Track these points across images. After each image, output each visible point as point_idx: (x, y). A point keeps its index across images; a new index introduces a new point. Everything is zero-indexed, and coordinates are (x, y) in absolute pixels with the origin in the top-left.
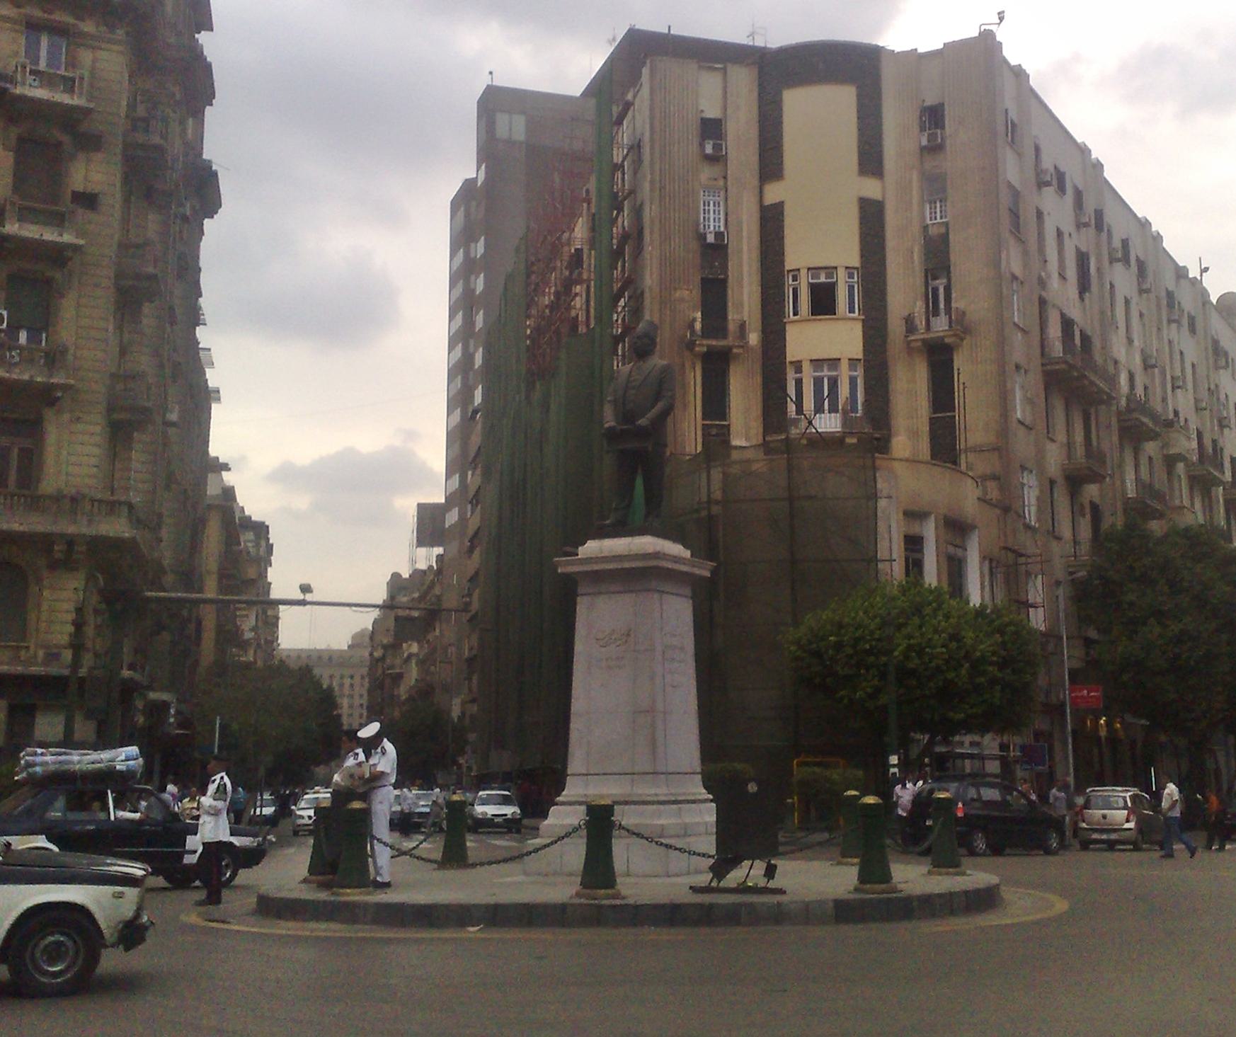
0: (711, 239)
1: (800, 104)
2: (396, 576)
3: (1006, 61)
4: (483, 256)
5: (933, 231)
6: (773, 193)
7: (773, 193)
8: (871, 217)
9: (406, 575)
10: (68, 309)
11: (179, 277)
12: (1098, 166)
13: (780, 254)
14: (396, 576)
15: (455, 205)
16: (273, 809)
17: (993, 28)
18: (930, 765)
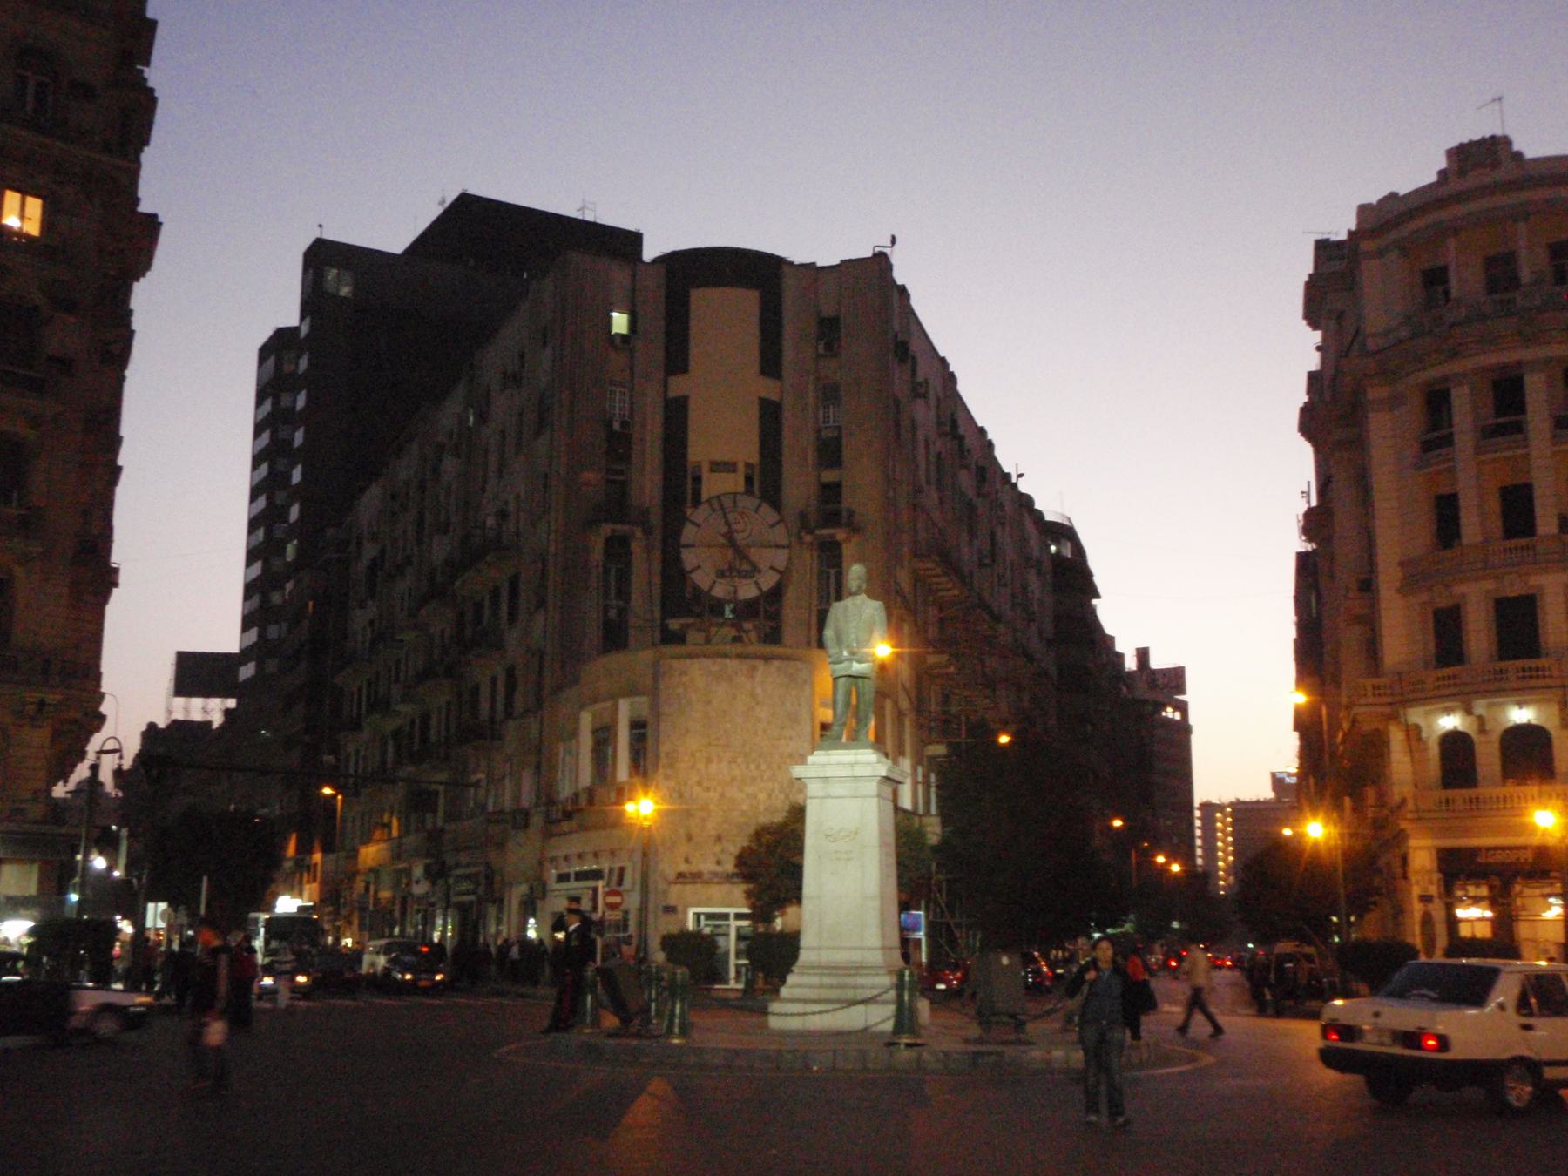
0: (616, 426)
1: (705, 302)
2: (152, 727)
3: (893, 281)
4: (303, 410)
5: (826, 434)
6: (678, 386)
7: (678, 386)
8: (770, 413)
9: (162, 724)
10: (1368, 916)
11: (541, 654)
12: (990, 445)
13: (683, 445)
14: (152, 727)
15: (265, 352)
16: (436, 940)
17: (887, 251)
18: (1220, 878)
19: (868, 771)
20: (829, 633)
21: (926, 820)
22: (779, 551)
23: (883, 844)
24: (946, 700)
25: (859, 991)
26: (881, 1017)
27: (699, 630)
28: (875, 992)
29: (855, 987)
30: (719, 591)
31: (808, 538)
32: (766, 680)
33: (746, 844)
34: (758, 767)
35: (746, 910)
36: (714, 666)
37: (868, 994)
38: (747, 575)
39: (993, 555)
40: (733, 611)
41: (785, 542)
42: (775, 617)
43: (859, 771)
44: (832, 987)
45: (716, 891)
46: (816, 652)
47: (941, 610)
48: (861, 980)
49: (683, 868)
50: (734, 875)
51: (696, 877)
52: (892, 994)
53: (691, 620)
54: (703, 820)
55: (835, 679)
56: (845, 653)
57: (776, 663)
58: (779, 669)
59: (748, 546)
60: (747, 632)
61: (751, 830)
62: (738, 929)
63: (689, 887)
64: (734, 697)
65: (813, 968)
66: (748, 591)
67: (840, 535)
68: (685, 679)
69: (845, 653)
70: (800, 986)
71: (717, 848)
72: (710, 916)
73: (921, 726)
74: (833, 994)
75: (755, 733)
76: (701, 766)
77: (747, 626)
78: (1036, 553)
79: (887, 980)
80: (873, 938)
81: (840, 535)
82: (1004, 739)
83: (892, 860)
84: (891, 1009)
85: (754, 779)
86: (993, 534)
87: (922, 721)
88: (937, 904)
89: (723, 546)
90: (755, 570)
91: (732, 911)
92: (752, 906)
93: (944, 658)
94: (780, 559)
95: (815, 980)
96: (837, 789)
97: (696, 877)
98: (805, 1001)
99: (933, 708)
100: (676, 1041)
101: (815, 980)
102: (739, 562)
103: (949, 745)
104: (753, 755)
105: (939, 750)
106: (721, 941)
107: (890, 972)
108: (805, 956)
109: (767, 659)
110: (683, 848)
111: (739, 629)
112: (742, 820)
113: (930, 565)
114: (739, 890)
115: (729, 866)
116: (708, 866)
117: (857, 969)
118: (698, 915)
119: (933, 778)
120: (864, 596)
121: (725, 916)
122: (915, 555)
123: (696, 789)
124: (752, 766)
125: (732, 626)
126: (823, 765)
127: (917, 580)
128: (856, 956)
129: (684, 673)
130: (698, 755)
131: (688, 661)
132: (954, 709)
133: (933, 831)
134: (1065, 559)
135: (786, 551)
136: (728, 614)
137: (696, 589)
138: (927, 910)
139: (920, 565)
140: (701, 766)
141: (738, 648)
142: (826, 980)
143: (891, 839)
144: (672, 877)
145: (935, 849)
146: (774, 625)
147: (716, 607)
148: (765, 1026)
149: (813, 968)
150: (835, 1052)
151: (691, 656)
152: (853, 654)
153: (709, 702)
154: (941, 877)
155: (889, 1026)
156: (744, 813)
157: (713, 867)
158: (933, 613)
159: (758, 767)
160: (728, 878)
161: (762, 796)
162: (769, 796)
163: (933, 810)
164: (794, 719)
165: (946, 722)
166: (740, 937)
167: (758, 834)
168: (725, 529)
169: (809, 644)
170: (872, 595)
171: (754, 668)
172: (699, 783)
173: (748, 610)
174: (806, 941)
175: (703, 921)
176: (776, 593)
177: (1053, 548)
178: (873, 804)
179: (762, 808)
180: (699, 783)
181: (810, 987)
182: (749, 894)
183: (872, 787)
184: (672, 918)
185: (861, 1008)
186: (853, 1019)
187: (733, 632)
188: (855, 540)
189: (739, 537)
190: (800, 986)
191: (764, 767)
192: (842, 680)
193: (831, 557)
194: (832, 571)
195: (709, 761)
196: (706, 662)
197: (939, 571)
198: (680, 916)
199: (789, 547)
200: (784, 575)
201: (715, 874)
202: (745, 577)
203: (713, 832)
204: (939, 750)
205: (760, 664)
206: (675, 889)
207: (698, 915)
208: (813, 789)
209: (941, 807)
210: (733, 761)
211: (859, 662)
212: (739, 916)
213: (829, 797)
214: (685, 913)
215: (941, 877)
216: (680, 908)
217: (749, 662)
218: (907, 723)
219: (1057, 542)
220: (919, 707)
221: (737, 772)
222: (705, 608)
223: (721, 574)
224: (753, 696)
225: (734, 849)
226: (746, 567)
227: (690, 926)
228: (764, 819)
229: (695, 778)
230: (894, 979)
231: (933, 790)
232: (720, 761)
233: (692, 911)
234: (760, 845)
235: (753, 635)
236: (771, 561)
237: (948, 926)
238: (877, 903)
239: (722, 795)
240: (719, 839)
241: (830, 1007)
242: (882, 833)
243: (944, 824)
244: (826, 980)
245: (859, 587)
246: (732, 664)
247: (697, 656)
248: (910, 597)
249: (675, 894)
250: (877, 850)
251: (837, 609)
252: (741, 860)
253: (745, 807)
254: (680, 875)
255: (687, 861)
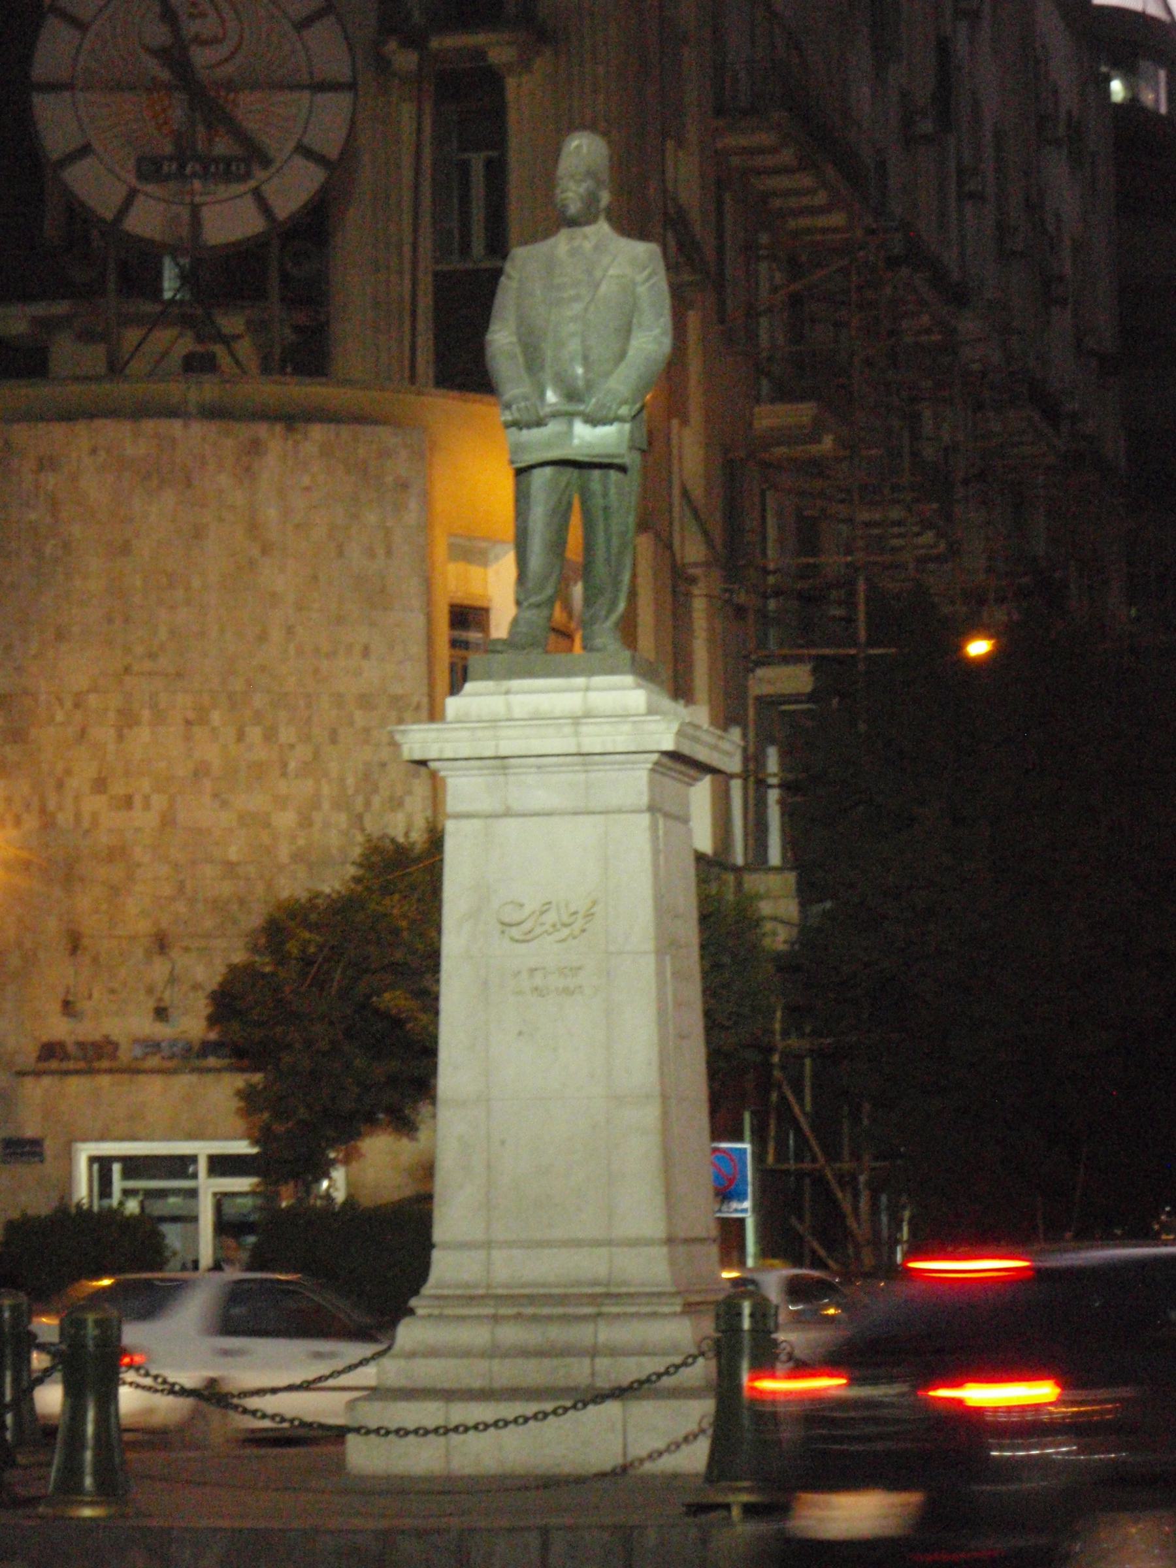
19: (620, 738)
20: (502, 338)
21: (755, 882)
22: (322, 98)
23: (666, 945)
24: (807, 536)
25: (602, 1363)
26: (669, 1436)
27: (87, 336)
28: (659, 1364)
29: (593, 1352)
30: (148, 219)
31: (405, 60)
32: (292, 481)
33: (239, 957)
34: (270, 735)
35: (242, 1147)
36: (132, 440)
37: (631, 1370)
38: (227, 171)
39: (946, 121)
40: (186, 278)
41: (340, 69)
42: (310, 297)
43: (594, 739)
44: (524, 1353)
45: (156, 1093)
46: (446, 409)
47: (795, 268)
48: (606, 1334)
49: (59, 1029)
50: (207, 1049)
51: (96, 1056)
52: (702, 1370)
53: (61, 308)
54: (115, 891)
55: (521, 472)
56: (551, 396)
57: (318, 432)
58: (326, 451)
59: (230, 85)
60: (227, 341)
61: (254, 920)
62: (220, 1199)
63: (75, 1085)
64: (198, 533)
65: (472, 1299)
66: (230, 219)
67: (499, 50)
68: (50, 480)
69: (551, 396)
70: (433, 1353)
71: (159, 970)
72: (134, 1166)
73: (740, 612)
74: (533, 1373)
75: (263, 637)
76: (104, 733)
77: (232, 323)
78: (1069, 101)
79: (681, 1332)
80: (641, 1211)
81: (499, 50)
82: (978, 648)
83: (693, 992)
84: (700, 1410)
85: (259, 771)
86: (943, 48)
87: (742, 598)
88: (786, 1117)
89: (154, 86)
90: (255, 155)
91: (203, 1149)
92: (262, 1137)
93: (803, 413)
94: (328, 121)
95: (476, 1335)
96: (537, 792)
97: (96, 1056)
98: (449, 1395)
99: (773, 556)
100: (87, 1512)
101: (476, 1335)
102: (205, 133)
103: (820, 665)
104: (259, 701)
105: (791, 679)
106: (172, 1235)
107: (690, 1309)
108: (446, 1268)
109: (292, 419)
110: (58, 973)
111: (206, 331)
112: (226, 889)
113: (766, 138)
114: (222, 1091)
115: (192, 1024)
116: (130, 1024)
117: (604, 1300)
118: (103, 1164)
119: (773, 763)
120: (603, 227)
121: (181, 1166)
122: (719, 112)
123: (94, 803)
124: (255, 734)
125: (186, 321)
126: (494, 722)
127: (723, 180)
128: (589, 1266)
129: (47, 464)
130: (93, 700)
131: (58, 430)
132: (833, 562)
133: (778, 904)
134: (1150, 115)
135: (343, 100)
136: (170, 286)
137: (77, 213)
138: (760, 1140)
139: (733, 141)
140: (104, 733)
141: (208, 390)
142: (511, 1334)
143: (689, 932)
144: (28, 1056)
145: (787, 965)
146: (338, 318)
147: (137, 268)
148: (340, 1464)
149: (472, 1299)
150: (545, 1531)
151: (68, 416)
152: (572, 395)
153: (125, 549)
154: (794, 1042)
155: (695, 1458)
156: (230, 868)
157: (143, 1024)
158: (769, 276)
159: (270, 735)
160: (191, 1057)
161: (286, 819)
162: (306, 822)
163: (775, 856)
164: (376, 596)
165: (808, 599)
166: (223, 1227)
167: (276, 931)
168: (159, 34)
169: (413, 379)
170: (631, 224)
171: (255, 447)
172: (100, 785)
173: (229, 277)
174: (451, 1221)
175: (118, 1184)
176: (313, 227)
177: (1117, 88)
178: (637, 833)
179: (284, 853)
180: (100, 785)
181: (466, 1353)
182: (250, 1100)
183: (636, 783)
184: (25, 1171)
185: (612, 1408)
186: (587, 1441)
187: (186, 344)
188: (541, 64)
189: (201, 57)
190: (433, 1353)
191: (286, 734)
192: (541, 477)
193: (470, 109)
194: (477, 162)
195: (127, 719)
196: (116, 433)
197: (787, 156)
198: (50, 1167)
199: (352, 86)
200: (339, 169)
201: (153, 1046)
202: (228, 177)
203: (144, 926)
204: (791, 679)
205: (273, 438)
206: (35, 1091)
207: (103, 1164)
208: (464, 790)
209: (790, 842)
210: (197, 719)
211: (593, 421)
212: (221, 1165)
213: (508, 814)
214: (68, 1158)
215: (794, 1042)
216: (50, 1147)
217: (245, 431)
218: (699, 605)
219: (1131, 76)
220: (734, 556)
221: (211, 754)
222: (98, 270)
223: (150, 169)
224: (254, 528)
225: (207, 973)
226: (223, 146)
227: (82, 1189)
228: (293, 886)
229: (84, 772)
230: (708, 1326)
231: (773, 795)
232: (159, 718)
233: (85, 1152)
234: (281, 959)
235: (244, 348)
236: (299, 130)
237: (819, 1180)
238: (650, 1115)
239: (167, 821)
240: (161, 944)
241: (549, 1406)
242: (663, 910)
243: (807, 892)
244: (511, 1334)
245: (591, 200)
246: (193, 436)
247: (90, 415)
248: (701, 231)
249: (35, 1105)
250: (648, 965)
251: (525, 264)
252: (226, 1003)
253: (233, 853)
254: (51, 1051)
255: (68, 1008)
